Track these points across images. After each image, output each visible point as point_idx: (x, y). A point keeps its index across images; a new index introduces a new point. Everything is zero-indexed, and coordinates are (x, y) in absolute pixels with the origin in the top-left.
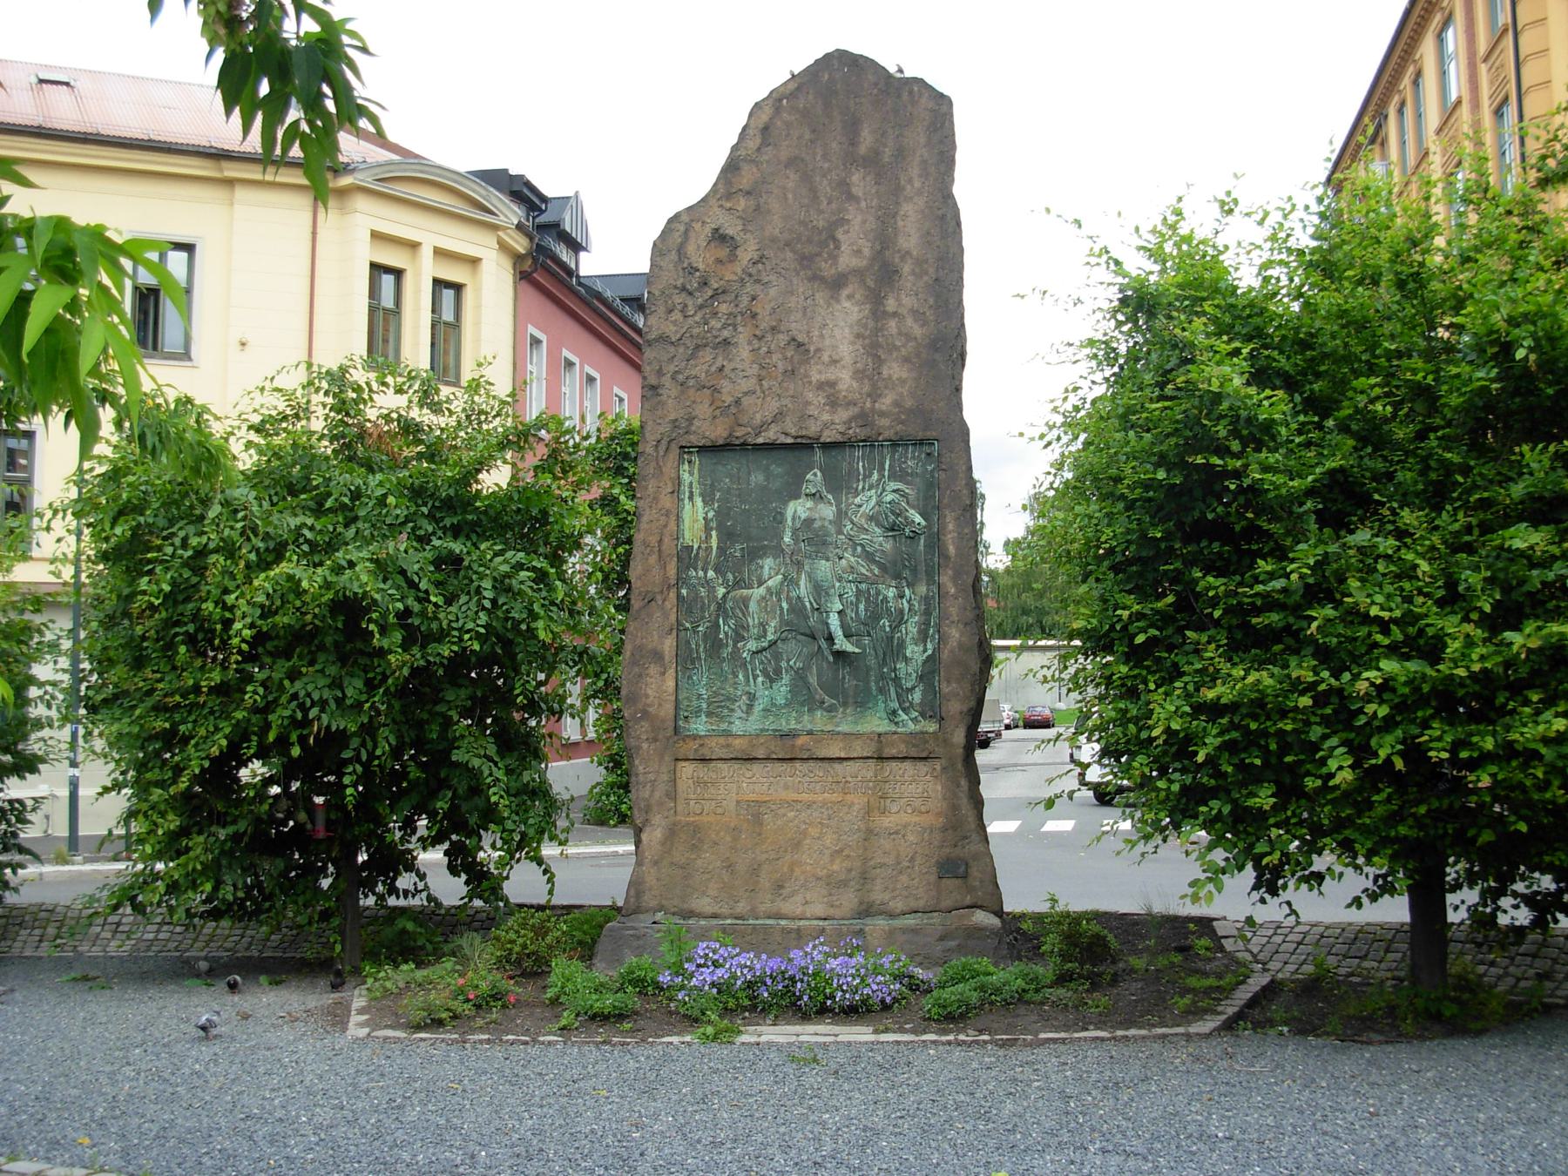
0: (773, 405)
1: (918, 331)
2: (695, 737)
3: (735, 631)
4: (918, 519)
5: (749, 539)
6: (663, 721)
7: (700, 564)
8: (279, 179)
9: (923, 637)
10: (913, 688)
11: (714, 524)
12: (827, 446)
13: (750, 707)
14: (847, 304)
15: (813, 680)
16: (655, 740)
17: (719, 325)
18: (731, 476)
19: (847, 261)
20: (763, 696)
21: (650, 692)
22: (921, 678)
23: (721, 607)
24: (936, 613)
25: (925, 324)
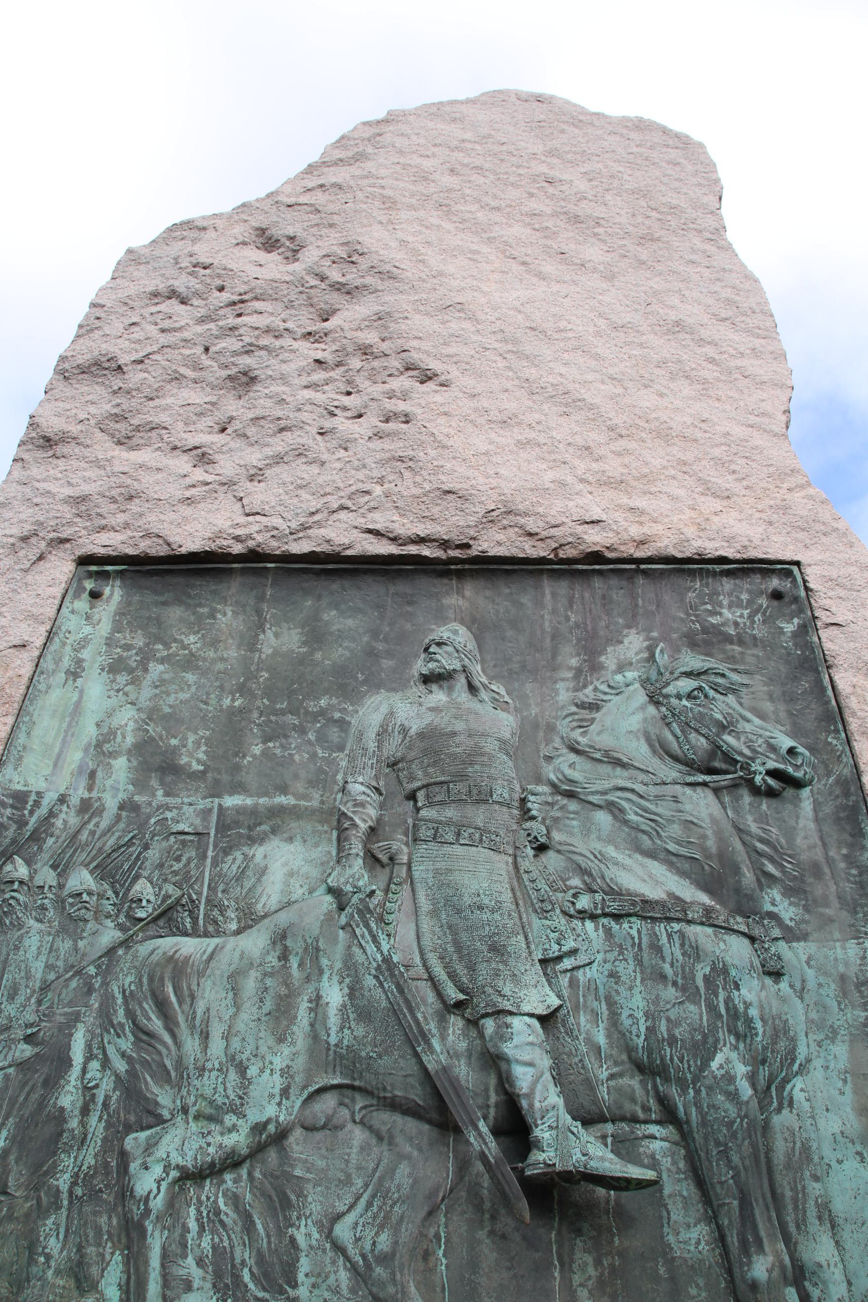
3: (129, 1087)
15: (775, 1104)
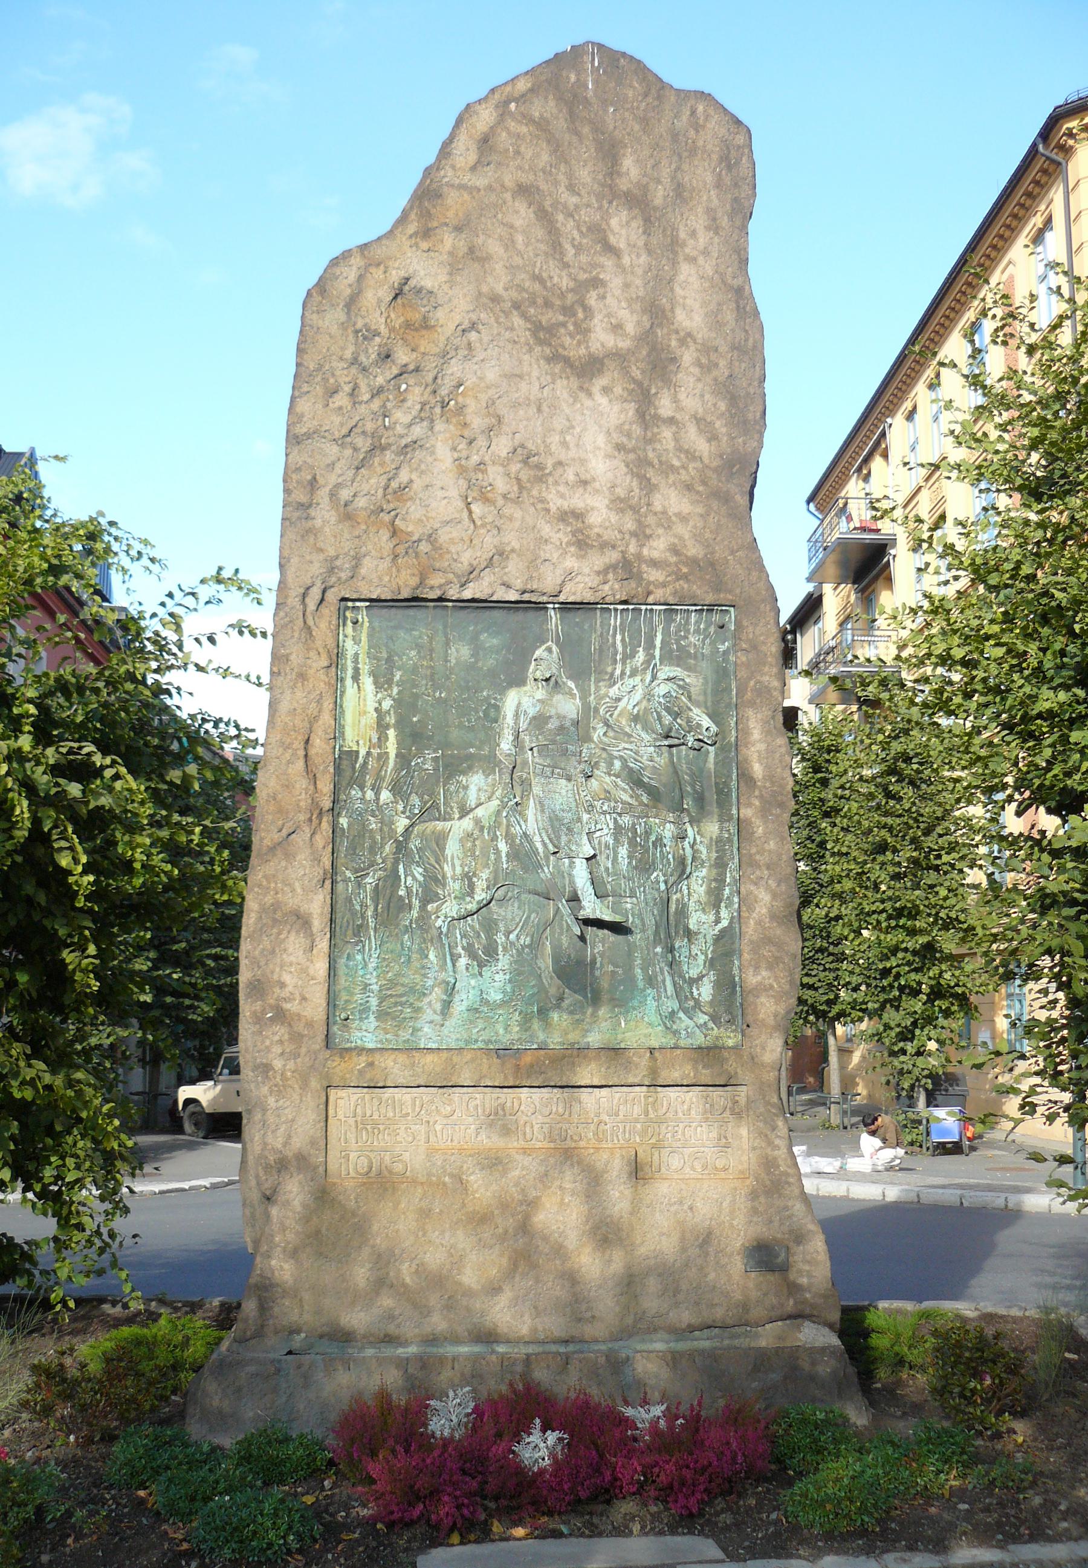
0: (489, 542)
1: (703, 447)
2: (361, 1050)
4: (706, 722)
5: (445, 745)
6: (310, 1024)
7: (369, 780)
8: (941, 1191)
9: (715, 900)
10: (701, 977)
11: (391, 719)
12: (567, 607)
13: (447, 1005)
14: (603, 401)
16: (296, 1055)
17: (406, 419)
18: (419, 647)
19: (601, 338)
20: (468, 990)
21: (287, 978)
22: (711, 963)
23: (401, 847)
24: (733, 865)
25: (713, 438)
